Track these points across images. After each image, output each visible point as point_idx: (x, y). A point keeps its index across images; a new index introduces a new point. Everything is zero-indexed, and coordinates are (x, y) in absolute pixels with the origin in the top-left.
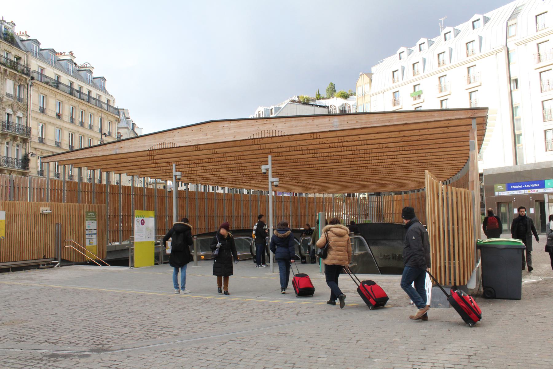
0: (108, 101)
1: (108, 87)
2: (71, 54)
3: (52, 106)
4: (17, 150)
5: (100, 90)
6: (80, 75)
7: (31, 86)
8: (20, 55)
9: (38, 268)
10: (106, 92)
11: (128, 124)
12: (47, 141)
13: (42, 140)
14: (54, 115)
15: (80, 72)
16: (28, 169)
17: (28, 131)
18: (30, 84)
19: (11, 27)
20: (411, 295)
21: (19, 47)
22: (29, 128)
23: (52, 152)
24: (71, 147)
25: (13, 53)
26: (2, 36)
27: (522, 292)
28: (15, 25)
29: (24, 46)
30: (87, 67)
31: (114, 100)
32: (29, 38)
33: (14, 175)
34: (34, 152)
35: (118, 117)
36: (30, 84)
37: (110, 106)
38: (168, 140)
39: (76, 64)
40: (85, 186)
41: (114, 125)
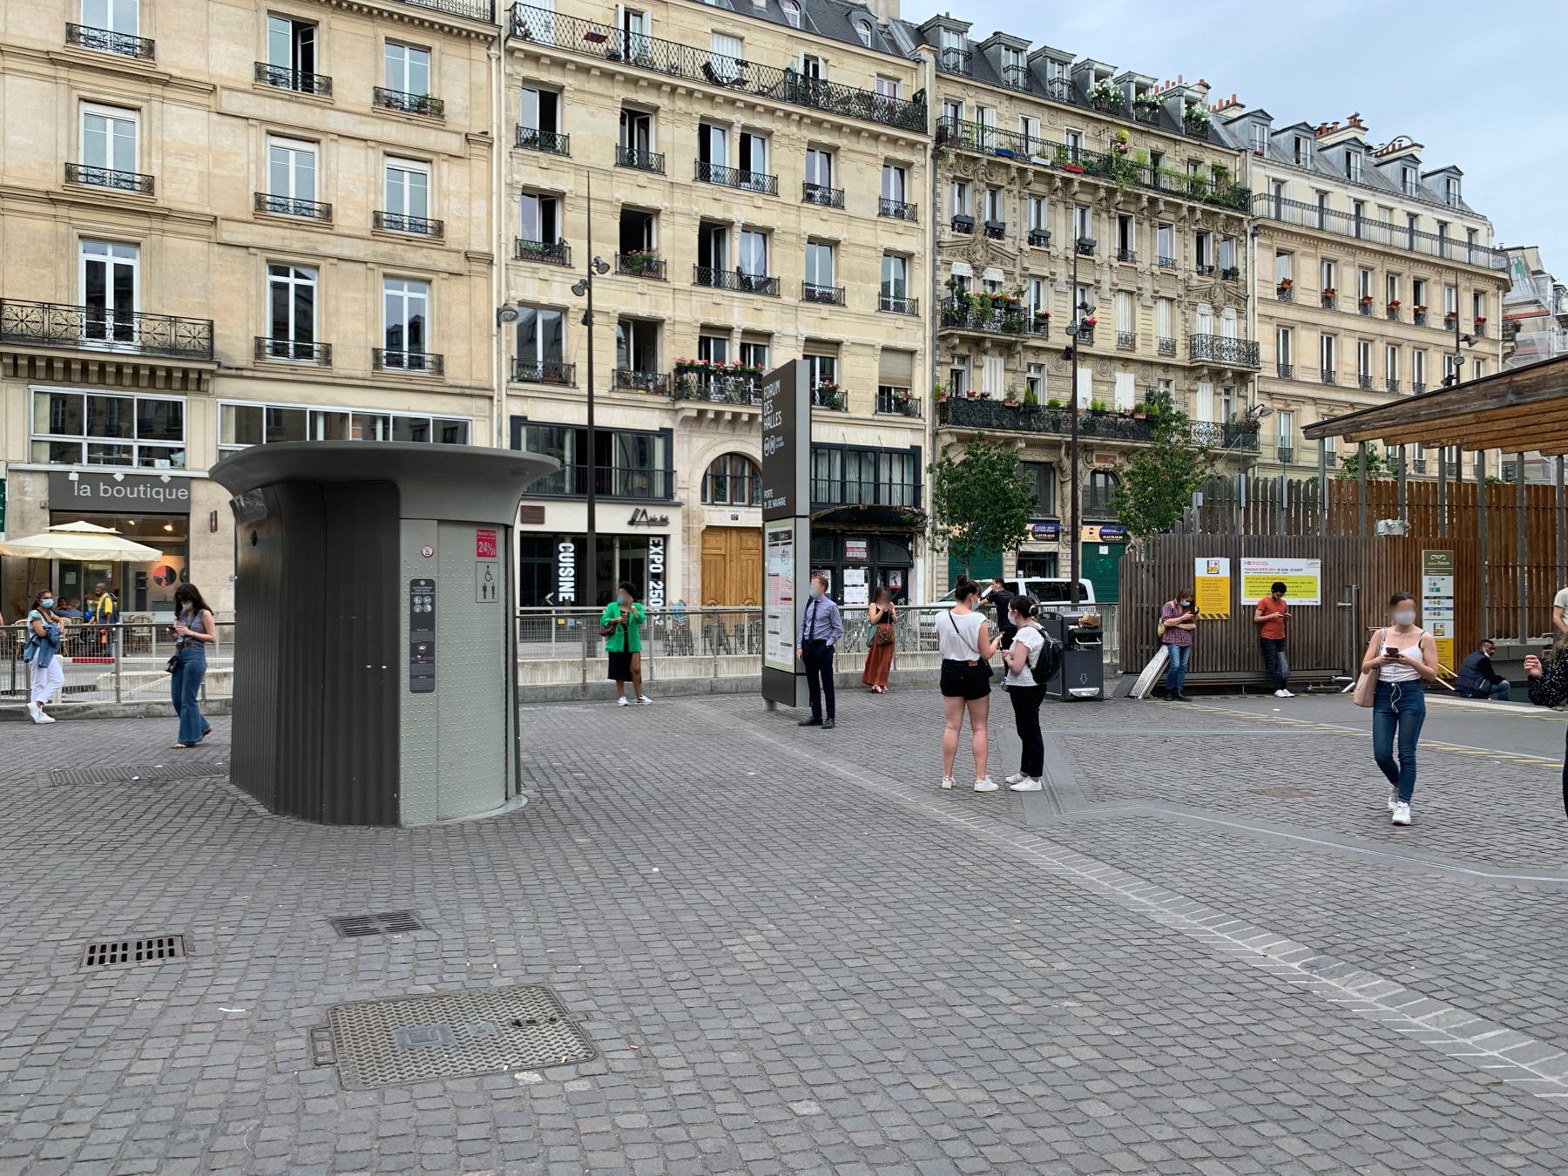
0: (1472, 232)
1: (1470, 191)
2: (1355, 122)
3: (1347, 284)
4: (1227, 401)
5: (1441, 207)
6: (1382, 177)
7: (1253, 235)
8: (1224, 161)
9: (1306, 692)
10: (1465, 212)
11: (1538, 289)
12: (1297, 374)
13: (1285, 371)
14: (1316, 300)
15: (1382, 169)
16: (1254, 448)
17: (1251, 352)
18: (1249, 231)
19: (1199, 96)
20: (1386, 765)
21: (1221, 143)
22: (658, 263)
23: (1352, 405)
24: (1419, 386)
25: (1208, 162)
26: (1182, 125)
27: (232, 593)
28: (1208, 87)
29: (1233, 135)
30: (1401, 149)
31: (1490, 228)
32: (1244, 111)
33: (1220, 467)
34: (1268, 404)
35: (1506, 276)
36: (1249, 231)
37: (1478, 248)
38: (432, 139)
39: (1369, 148)
40: (1537, 495)
41: (1492, 302)
